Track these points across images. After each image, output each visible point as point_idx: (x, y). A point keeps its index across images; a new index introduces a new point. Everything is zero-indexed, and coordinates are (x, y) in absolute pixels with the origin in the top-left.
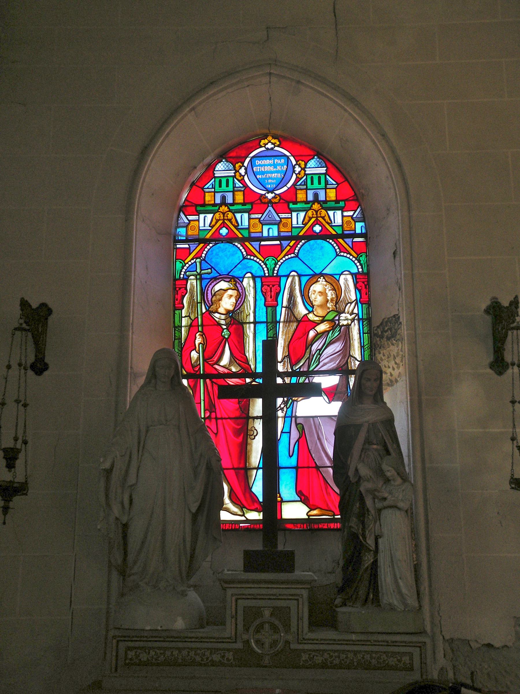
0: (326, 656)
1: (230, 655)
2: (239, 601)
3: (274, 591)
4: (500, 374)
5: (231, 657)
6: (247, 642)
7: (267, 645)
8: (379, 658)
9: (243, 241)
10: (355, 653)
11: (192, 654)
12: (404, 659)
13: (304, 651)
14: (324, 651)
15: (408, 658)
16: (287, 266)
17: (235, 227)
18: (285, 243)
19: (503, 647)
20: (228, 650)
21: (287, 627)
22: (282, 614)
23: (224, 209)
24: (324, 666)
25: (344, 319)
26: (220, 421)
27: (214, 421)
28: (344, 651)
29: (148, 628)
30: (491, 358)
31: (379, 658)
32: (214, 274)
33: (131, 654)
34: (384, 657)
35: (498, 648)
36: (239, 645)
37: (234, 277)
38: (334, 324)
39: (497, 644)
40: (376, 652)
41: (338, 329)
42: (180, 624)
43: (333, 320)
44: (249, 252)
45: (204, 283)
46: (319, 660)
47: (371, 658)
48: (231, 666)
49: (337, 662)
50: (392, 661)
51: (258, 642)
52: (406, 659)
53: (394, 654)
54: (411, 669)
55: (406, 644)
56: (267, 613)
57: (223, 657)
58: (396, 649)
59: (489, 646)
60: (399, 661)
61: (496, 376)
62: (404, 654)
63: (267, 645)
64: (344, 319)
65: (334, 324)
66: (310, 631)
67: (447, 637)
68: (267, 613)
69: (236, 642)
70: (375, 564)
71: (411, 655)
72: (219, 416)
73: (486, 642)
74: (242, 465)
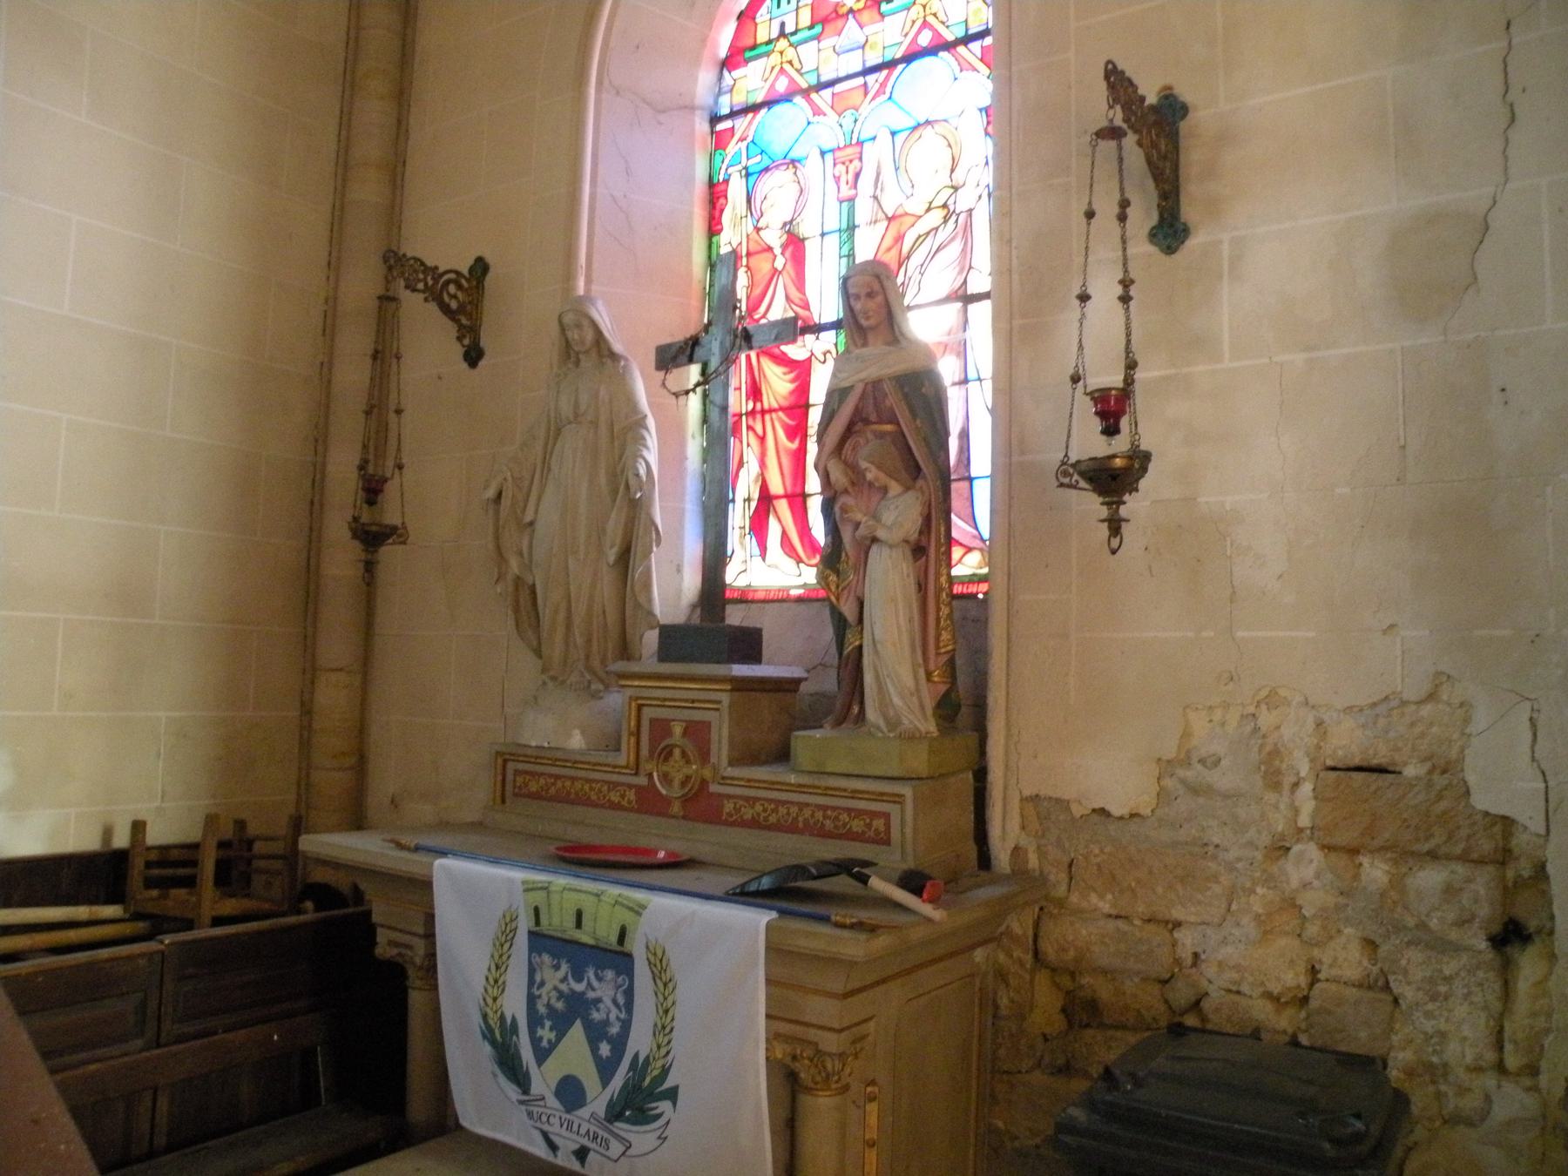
0: (759, 808)
1: (631, 795)
2: (645, 710)
3: (658, 693)
4: (1170, 250)
5: (633, 797)
6: (650, 776)
7: (676, 783)
8: (836, 818)
9: (806, 93)
10: (802, 806)
11: (587, 787)
12: (875, 823)
13: (729, 797)
14: (756, 799)
15: (882, 821)
16: (876, 117)
17: (798, 71)
18: (871, 79)
19: (1132, 816)
20: (630, 786)
21: (704, 756)
22: (698, 732)
23: (783, 43)
24: (754, 824)
25: (964, 201)
26: (767, 417)
27: (759, 416)
28: (784, 803)
29: (533, 744)
30: (1154, 219)
31: (836, 818)
32: (766, 162)
33: (520, 780)
34: (844, 817)
35: (1121, 818)
36: (642, 781)
37: (793, 162)
38: (948, 212)
39: (1116, 811)
40: (834, 808)
41: (954, 218)
42: (576, 741)
43: (945, 206)
44: (817, 112)
45: (752, 179)
46: (748, 813)
47: (825, 817)
48: (631, 810)
49: (773, 819)
50: (857, 825)
51: (666, 779)
52: (879, 823)
53: (859, 813)
54: (887, 842)
55: (880, 797)
56: (678, 729)
57: (623, 796)
58: (862, 805)
59: (1103, 812)
60: (869, 826)
61: (1163, 256)
62: (874, 815)
63: (676, 783)
64: (964, 201)
65: (948, 212)
66: (731, 764)
67: (1027, 793)
68: (678, 729)
69: (636, 774)
70: (860, 647)
71: (887, 816)
72: (766, 406)
73: (1097, 806)
74: (798, 491)
